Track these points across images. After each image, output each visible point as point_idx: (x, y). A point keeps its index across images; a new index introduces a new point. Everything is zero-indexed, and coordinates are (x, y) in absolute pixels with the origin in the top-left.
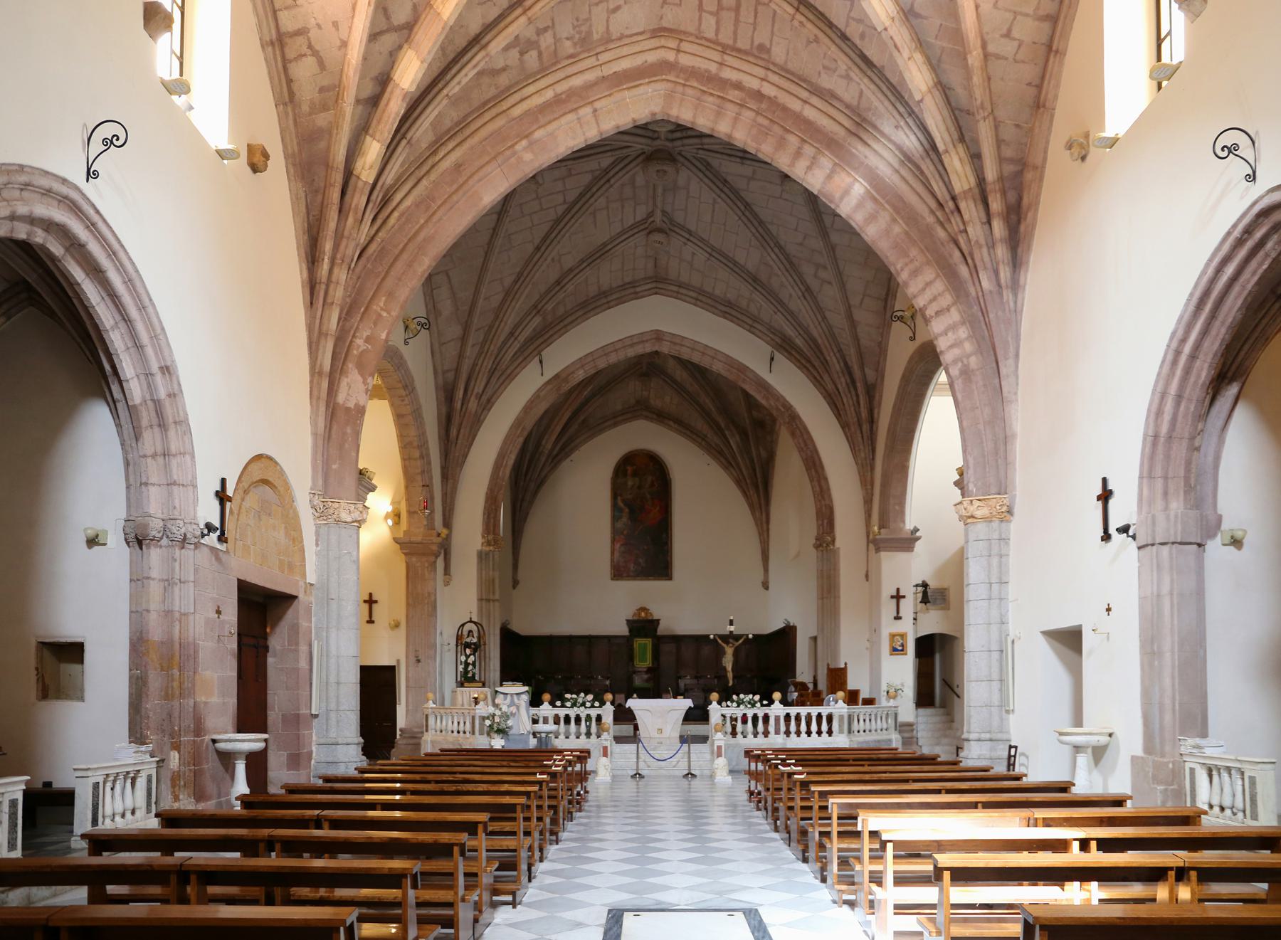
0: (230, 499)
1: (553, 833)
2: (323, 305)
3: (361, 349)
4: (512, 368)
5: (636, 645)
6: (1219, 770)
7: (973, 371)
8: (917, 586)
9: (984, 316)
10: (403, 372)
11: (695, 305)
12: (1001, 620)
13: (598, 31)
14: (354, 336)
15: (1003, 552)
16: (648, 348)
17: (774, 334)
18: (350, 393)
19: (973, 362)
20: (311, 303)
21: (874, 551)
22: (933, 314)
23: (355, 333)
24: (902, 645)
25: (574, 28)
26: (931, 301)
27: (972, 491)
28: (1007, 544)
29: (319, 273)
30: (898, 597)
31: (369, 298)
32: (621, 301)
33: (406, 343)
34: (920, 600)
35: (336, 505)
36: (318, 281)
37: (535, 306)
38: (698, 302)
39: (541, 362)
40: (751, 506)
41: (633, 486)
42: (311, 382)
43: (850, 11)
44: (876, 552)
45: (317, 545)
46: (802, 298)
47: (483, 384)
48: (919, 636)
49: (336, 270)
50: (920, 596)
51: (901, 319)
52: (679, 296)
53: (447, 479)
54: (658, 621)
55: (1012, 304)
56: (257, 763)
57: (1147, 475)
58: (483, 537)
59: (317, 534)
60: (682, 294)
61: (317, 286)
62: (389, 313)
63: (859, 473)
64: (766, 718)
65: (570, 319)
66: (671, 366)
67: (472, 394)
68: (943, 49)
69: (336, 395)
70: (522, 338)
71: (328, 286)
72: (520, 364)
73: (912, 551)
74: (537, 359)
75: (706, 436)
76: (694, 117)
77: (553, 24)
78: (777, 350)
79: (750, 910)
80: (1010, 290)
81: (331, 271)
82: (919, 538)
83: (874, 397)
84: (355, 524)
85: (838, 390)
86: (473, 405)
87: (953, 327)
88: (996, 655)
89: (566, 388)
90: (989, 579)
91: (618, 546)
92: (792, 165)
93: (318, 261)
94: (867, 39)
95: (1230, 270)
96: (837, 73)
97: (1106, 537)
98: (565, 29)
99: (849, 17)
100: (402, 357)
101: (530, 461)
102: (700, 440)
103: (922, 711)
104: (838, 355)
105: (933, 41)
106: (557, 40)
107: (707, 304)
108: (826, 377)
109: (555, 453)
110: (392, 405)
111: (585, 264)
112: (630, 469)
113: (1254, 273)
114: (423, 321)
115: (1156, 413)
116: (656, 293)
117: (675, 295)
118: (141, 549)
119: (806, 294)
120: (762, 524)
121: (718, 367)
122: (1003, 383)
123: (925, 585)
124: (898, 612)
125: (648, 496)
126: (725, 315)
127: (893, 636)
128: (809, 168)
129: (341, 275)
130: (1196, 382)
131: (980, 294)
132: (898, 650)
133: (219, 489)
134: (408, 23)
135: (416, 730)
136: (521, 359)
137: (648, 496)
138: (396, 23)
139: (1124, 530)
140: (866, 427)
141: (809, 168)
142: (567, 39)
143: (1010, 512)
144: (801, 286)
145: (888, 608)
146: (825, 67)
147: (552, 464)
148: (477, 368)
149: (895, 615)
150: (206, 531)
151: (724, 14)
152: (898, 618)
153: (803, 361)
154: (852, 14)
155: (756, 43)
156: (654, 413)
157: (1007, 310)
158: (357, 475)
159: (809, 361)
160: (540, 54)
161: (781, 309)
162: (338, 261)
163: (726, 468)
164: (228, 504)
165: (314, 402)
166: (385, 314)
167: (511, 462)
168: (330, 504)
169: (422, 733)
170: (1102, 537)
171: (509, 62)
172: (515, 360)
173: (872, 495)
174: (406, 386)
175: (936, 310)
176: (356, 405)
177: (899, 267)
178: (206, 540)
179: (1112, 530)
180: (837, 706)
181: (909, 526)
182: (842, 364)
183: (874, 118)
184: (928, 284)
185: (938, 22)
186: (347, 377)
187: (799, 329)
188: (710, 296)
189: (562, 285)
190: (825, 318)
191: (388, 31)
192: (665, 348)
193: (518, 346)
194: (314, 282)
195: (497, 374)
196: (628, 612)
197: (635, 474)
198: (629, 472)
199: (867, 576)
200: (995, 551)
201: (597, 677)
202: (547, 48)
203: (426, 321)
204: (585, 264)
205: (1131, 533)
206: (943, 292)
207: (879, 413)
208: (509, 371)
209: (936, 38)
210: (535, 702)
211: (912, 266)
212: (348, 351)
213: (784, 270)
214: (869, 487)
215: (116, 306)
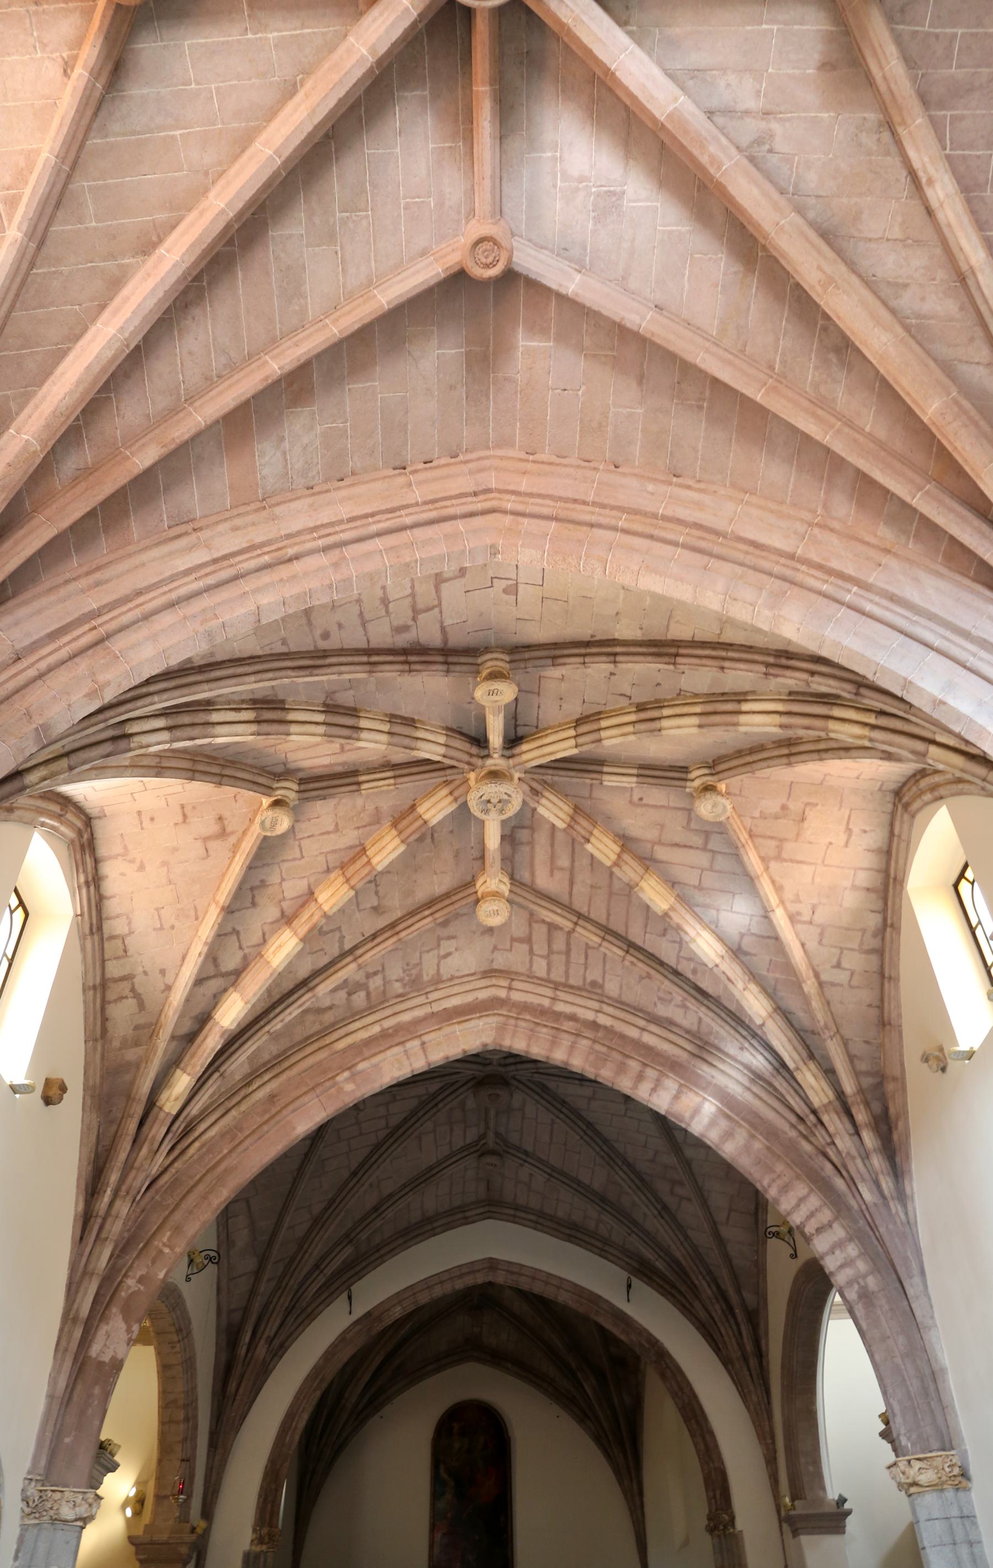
2: (95, 1241)
10: (179, 1312)
13: (428, 972)
14: (125, 1276)
16: (480, 1279)
20: (81, 1238)
21: (791, 1535)
23: (127, 1272)
25: (404, 971)
29: (97, 1207)
31: (152, 1231)
32: (448, 1227)
33: (188, 1279)
37: (347, 1235)
39: (350, 1298)
43: (680, 951)
49: (118, 1203)
51: (777, 1235)
61: (93, 1219)
62: (172, 1249)
67: (260, 1338)
68: (777, 980)
70: (328, 1272)
71: (105, 1219)
74: (345, 1295)
76: (528, 1045)
77: (383, 969)
80: (896, 1202)
81: (111, 1204)
82: (849, 1513)
86: (261, 1351)
87: (839, 1245)
92: (635, 1087)
94: (699, 974)
96: (673, 1003)
98: (395, 971)
99: (678, 957)
104: (708, 1278)
105: (766, 973)
106: (386, 982)
111: (408, 1189)
114: (212, 1254)
116: (489, 1218)
122: (913, 1306)
126: (570, 1239)
128: (654, 1090)
131: (864, 1207)
134: (236, 970)
138: (224, 970)
140: (753, 1362)
141: (654, 1090)
142: (397, 981)
143: (965, 1475)
146: (660, 999)
148: (271, 1307)
151: (555, 957)
153: (667, 1287)
154: (682, 954)
155: (588, 980)
159: (674, 1286)
160: (368, 994)
161: (635, 1230)
166: (167, 1250)
168: (50, 1494)
171: (336, 1002)
177: (765, 1183)
183: (716, 1042)
184: (801, 1200)
185: (767, 958)
191: (214, 976)
202: (377, 988)
204: (408, 1189)
206: (821, 1207)
209: (768, 970)
211: (780, 1182)
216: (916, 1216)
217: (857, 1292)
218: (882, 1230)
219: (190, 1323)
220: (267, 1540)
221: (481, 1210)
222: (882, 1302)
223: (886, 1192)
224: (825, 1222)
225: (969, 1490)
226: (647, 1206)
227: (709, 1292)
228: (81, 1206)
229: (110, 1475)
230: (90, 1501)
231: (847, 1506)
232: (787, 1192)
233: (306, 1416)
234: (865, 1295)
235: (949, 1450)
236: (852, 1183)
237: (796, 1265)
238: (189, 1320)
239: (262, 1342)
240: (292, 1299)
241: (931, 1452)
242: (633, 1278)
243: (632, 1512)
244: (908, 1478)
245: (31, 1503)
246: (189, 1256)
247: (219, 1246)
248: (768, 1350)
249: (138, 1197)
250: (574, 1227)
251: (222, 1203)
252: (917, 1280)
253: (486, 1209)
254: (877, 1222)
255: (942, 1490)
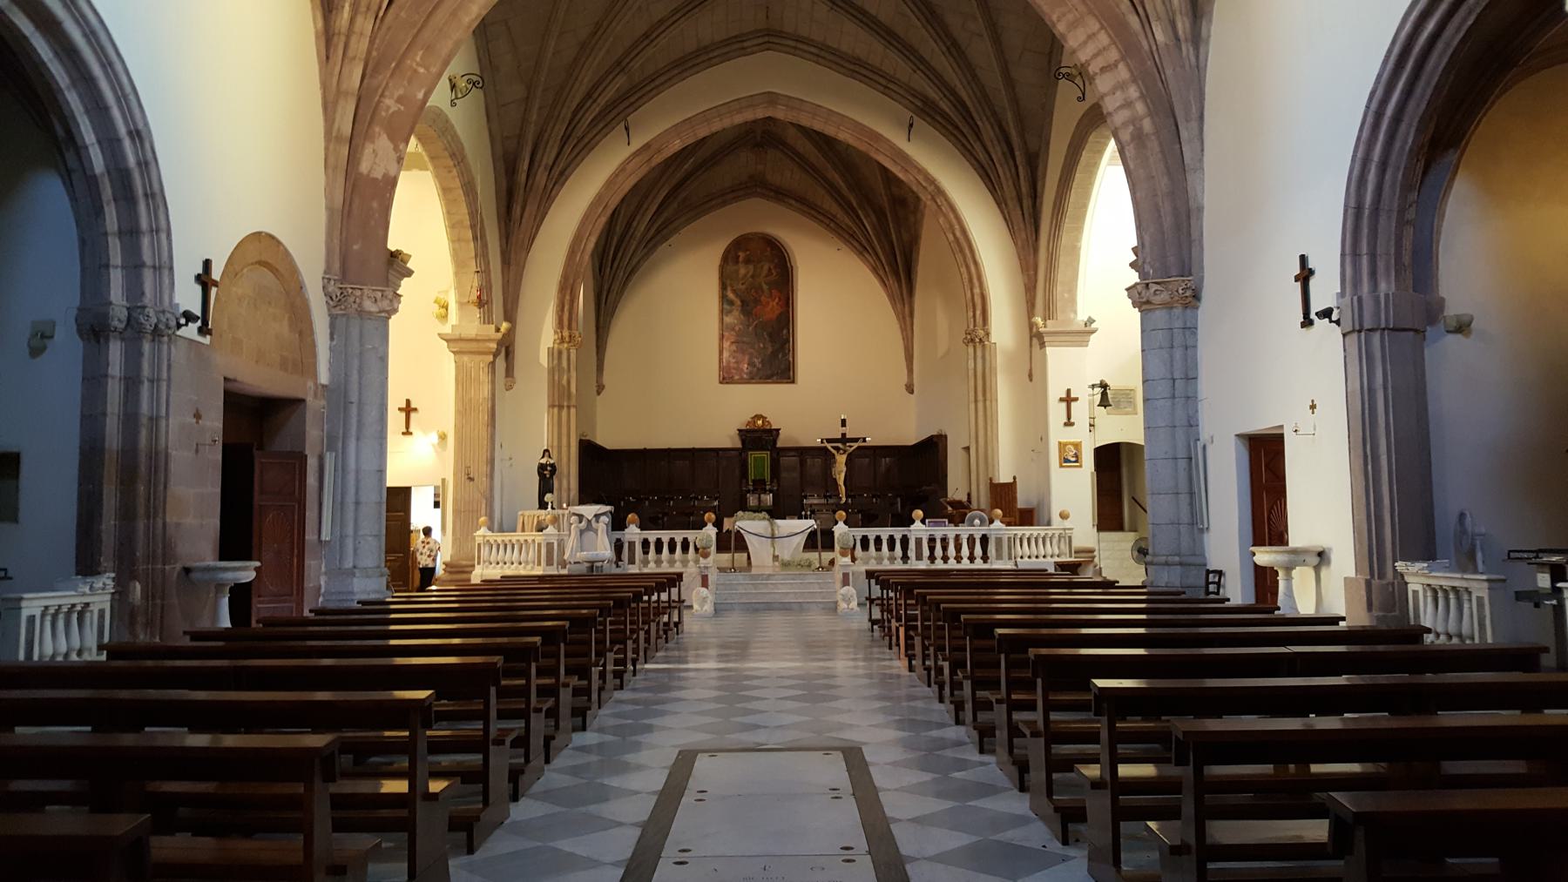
0: (215, 284)
1: (619, 675)
2: (343, 60)
3: (391, 111)
4: (590, 136)
5: (751, 461)
6: (1446, 592)
7: (1147, 135)
8: (1093, 386)
9: (1159, 73)
10: (449, 137)
11: (817, 63)
12: (1189, 421)
14: (382, 95)
15: (1190, 343)
16: (760, 113)
17: (913, 95)
18: (377, 161)
19: (1147, 125)
20: (328, 58)
21: (1038, 347)
22: (1098, 71)
23: (383, 92)
24: (1076, 456)
26: (1095, 56)
27: (1149, 273)
28: (1195, 334)
29: (337, 24)
30: (1068, 400)
31: (401, 52)
32: (726, 57)
33: (453, 104)
34: (1098, 403)
35: (358, 293)
36: (336, 31)
37: (619, 63)
38: (820, 59)
39: (627, 129)
40: (891, 297)
41: (745, 275)
42: (327, 149)
44: (1041, 348)
45: (332, 338)
46: (947, 54)
47: (553, 155)
48: (1097, 446)
49: (359, 20)
50: (1098, 398)
51: (1069, 77)
52: (798, 52)
53: (509, 264)
54: (778, 430)
55: (1193, 59)
56: (241, 596)
57: (1351, 251)
58: (556, 332)
59: (332, 326)
60: (800, 49)
61: (336, 38)
62: (427, 69)
63: (1019, 257)
64: (905, 541)
65: (662, 79)
66: (792, 136)
67: (539, 166)
69: (359, 164)
70: (602, 101)
71: (348, 37)
72: (600, 131)
73: (1087, 346)
74: (622, 124)
75: (835, 216)
78: (917, 115)
79: (851, 749)
80: (1189, 44)
81: (352, 21)
82: (1093, 332)
83: (1037, 167)
84: (383, 314)
85: (992, 160)
86: (541, 178)
87: (1121, 86)
88: (1182, 464)
89: (658, 159)
90: (1172, 374)
91: (726, 344)
93: (337, 9)
95: (1431, 25)
97: (1307, 322)
100: (447, 121)
101: (621, 241)
102: (827, 221)
103: (1105, 535)
104: (992, 120)
107: (830, 61)
108: (977, 146)
109: (649, 236)
110: (437, 176)
111: (679, 15)
112: (742, 255)
113: (1458, 30)
114: (475, 78)
115: (1357, 183)
116: (768, 49)
117: (792, 51)
118: (98, 342)
119: (952, 49)
120: (904, 318)
121: (844, 136)
122: (1184, 149)
123: (1104, 386)
124: (1069, 417)
125: (765, 287)
126: (853, 74)
127: (1062, 446)
129: (365, 25)
130: (1402, 148)
131: (1154, 48)
132: (1070, 462)
133: (200, 271)
135: (464, 563)
136: (601, 125)
137: (765, 287)
139: (1326, 314)
140: (1027, 203)
143: (1197, 296)
144: (946, 39)
145: (1056, 412)
147: (646, 250)
148: (546, 135)
149: (1066, 420)
150: (183, 321)
152: (1069, 423)
153: (950, 128)
156: (771, 190)
157: (1187, 67)
158: (389, 256)
159: (957, 127)
161: (922, 67)
162: (363, 9)
163: (860, 254)
164: (214, 291)
165: (330, 171)
166: (422, 70)
167: (591, 245)
168: (350, 291)
169: (473, 566)
170: (1301, 323)
172: (595, 125)
173: (1036, 281)
174: (454, 154)
175: (1101, 66)
176: (385, 175)
177: (1054, 18)
178: (182, 332)
179: (1313, 316)
180: (992, 526)
181: (1082, 316)
182: (997, 129)
184: (1091, 37)
186: (373, 142)
187: (943, 89)
188: (834, 52)
189: (651, 38)
190: (976, 75)
192: (780, 113)
193: (598, 109)
194: (331, 33)
195: (572, 142)
196: (741, 419)
197: (747, 261)
198: (741, 259)
199: (1030, 376)
200: (1178, 341)
201: (702, 498)
203: (480, 79)
204: (679, 15)
205: (1334, 317)
206: (1109, 45)
207: (1044, 186)
208: (586, 140)
210: (618, 524)
211: (1070, 17)
212: (374, 112)
213: (924, 21)
214: (1032, 273)
215: (74, 62)
216: (1206, 60)
217: (1132, 134)
218: (1169, 72)
219: (463, 149)
220: (567, 339)
221: (761, 40)
222: (1153, 145)
223: (1180, 32)
224: (1112, 61)
225: (1197, 308)
226: (936, 42)
227: (992, 134)
228: (320, 24)
229: (406, 279)
230: (390, 297)
231: (1093, 326)
232: (1076, 27)
233: (593, 240)
234: (1139, 137)
235: (1187, 277)
236: (1146, 21)
237: (1086, 105)
238: (462, 144)
239: (542, 168)
240: (567, 129)
241: (1170, 277)
242: (915, 117)
243: (903, 330)
244: (1142, 298)
245: (334, 297)
246: (450, 80)
247: (481, 70)
248: (1043, 192)
249: (381, 14)
250: (857, 61)
251: (473, 21)
252: (1194, 124)
253: (766, 39)
254: (1165, 65)
255: (1172, 308)
